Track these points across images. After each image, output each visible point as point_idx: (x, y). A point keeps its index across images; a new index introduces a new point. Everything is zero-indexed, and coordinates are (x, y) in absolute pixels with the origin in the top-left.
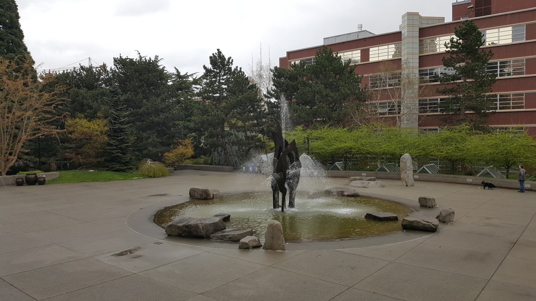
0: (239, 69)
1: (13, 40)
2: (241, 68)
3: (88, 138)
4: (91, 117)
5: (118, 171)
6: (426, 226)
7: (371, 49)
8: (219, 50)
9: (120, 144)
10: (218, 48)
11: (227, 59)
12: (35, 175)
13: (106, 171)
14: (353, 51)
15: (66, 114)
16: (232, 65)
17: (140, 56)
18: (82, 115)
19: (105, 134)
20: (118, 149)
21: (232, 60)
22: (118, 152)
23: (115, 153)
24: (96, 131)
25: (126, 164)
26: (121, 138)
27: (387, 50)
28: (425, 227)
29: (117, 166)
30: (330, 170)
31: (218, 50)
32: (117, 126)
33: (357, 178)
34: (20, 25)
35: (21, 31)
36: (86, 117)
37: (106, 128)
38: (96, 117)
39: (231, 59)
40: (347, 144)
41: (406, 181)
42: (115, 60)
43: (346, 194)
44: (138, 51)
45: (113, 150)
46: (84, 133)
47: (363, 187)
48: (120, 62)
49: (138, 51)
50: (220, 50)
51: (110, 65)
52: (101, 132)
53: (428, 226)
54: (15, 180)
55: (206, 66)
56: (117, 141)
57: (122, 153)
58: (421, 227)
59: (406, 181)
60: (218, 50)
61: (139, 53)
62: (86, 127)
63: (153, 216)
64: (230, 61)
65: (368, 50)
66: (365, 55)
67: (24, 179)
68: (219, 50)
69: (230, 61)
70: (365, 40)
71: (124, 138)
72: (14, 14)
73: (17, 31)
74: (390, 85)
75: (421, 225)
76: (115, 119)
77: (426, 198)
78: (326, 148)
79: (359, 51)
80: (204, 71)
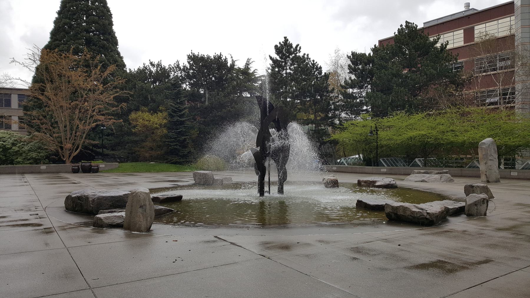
0: (306, 56)
1: (105, 45)
2: (308, 55)
3: (150, 130)
4: (154, 111)
5: (175, 163)
6: (416, 215)
7: (476, 28)
8: (286, 37)
9: (178, 137)
10: (285, 36)
11: (294, 46)
12: (97, 167)
13: (166, 163)
14: (455, 31)
15: (123, 105)
16: (299, 53)
17: (233, 60)
18: (146, 109)
19: (165, 127)
20: (177, 142)
21: (300, 48)
22: (176, 145)
23: (173, 145)
24: (156, 124)
25: (184, 156)
26: (180, 130)
27: (496, 27)
28: (414, 217)
29: (176, 159)
30: (411, 166)
31: (285, 38)
32: (176, 119)
33: (422, 171)
34: (115, 33)
35: (115, 38)
36: (149, 111)
37: (165, 121)
38: (159, 111)
39: (299, 47)
40: (423, 133)
41: (487, 174)
42: (189, 57)
43: (377, 184)
44: (231, 55)
45: (171, 142)
46: (145, 126)
47: (422, 182)
48: (194, 59)
49: (231, 55)
50: (287, 38)
51: (184, 62)
52: (161, 125)
53: (418, 215)
54: (71, 168)
55: (271, 56)
56: (175, 134)
57: (180, 146)
58: (410, 217)
59: (486, 175)
60: (285, 38)
61: (232, 57)
62: (147, 121)
63: (291, 228)
64: (298, 48)
65: (472, 29)
66: (469, 35)
67: (80, 167)
68: (286, 37)
69: (298, 49)
70: (469, 18)
71: (181, 131)
72: (107, 22)
73: (110, 37)
74: (501, 68)
75: (408, 213)
76: (175, 112)
77: (473, 185)
78: (395, 137)
79: (462, 31)
80: (271, 62)
